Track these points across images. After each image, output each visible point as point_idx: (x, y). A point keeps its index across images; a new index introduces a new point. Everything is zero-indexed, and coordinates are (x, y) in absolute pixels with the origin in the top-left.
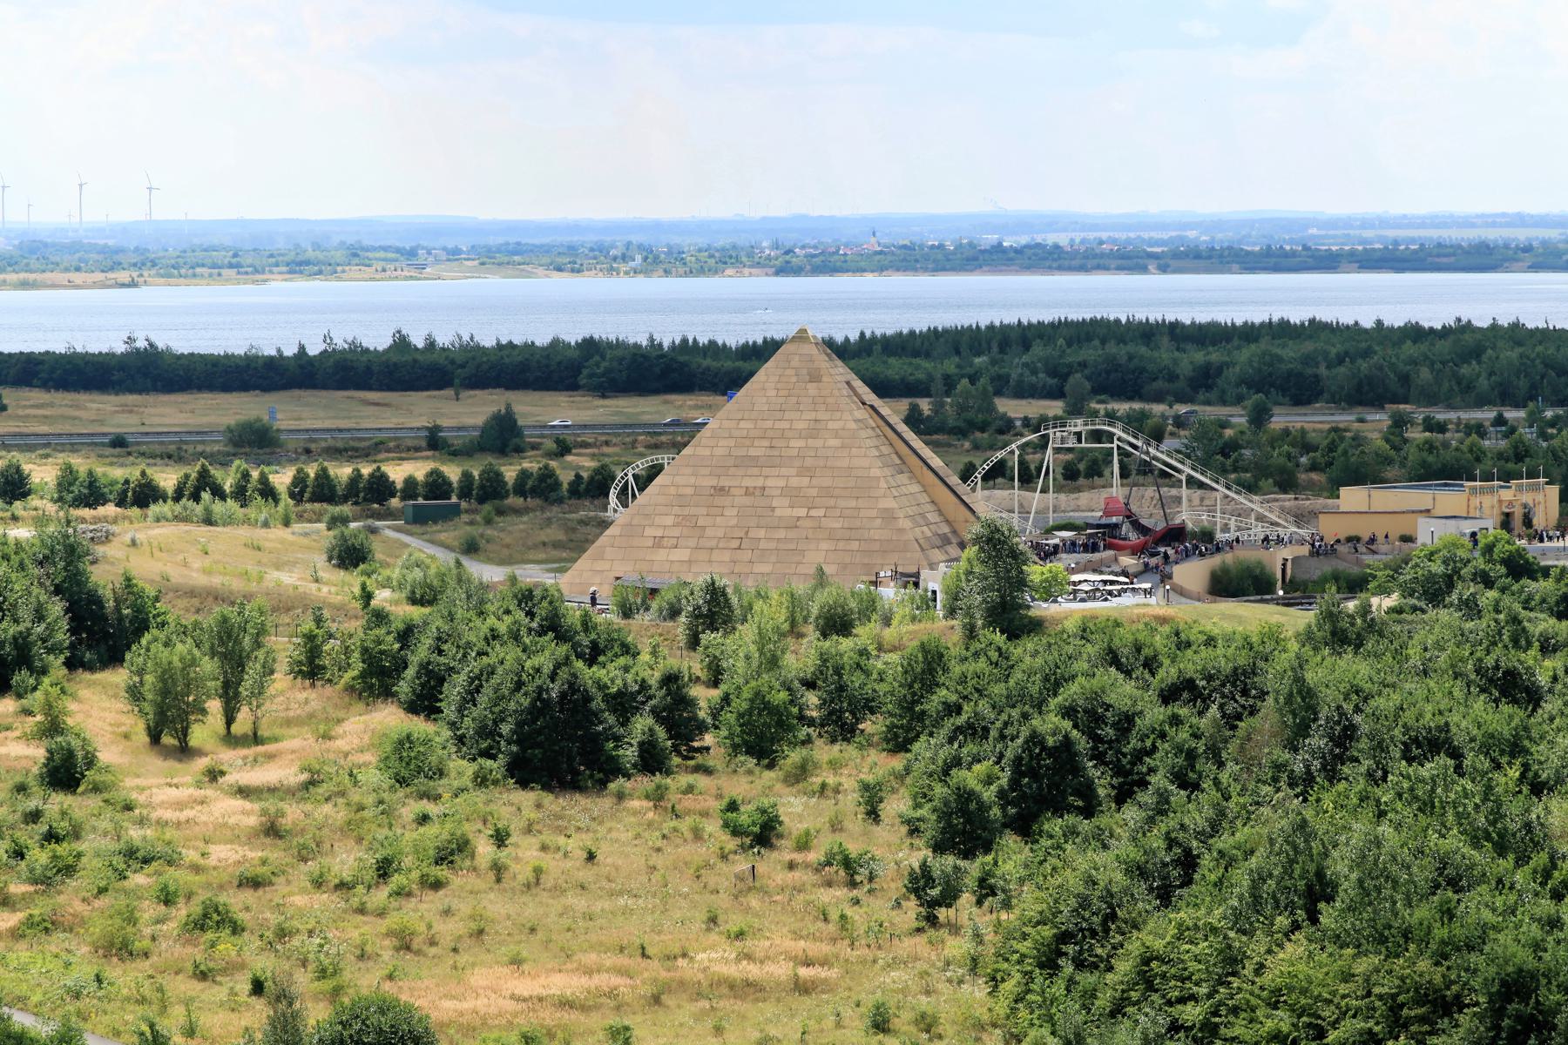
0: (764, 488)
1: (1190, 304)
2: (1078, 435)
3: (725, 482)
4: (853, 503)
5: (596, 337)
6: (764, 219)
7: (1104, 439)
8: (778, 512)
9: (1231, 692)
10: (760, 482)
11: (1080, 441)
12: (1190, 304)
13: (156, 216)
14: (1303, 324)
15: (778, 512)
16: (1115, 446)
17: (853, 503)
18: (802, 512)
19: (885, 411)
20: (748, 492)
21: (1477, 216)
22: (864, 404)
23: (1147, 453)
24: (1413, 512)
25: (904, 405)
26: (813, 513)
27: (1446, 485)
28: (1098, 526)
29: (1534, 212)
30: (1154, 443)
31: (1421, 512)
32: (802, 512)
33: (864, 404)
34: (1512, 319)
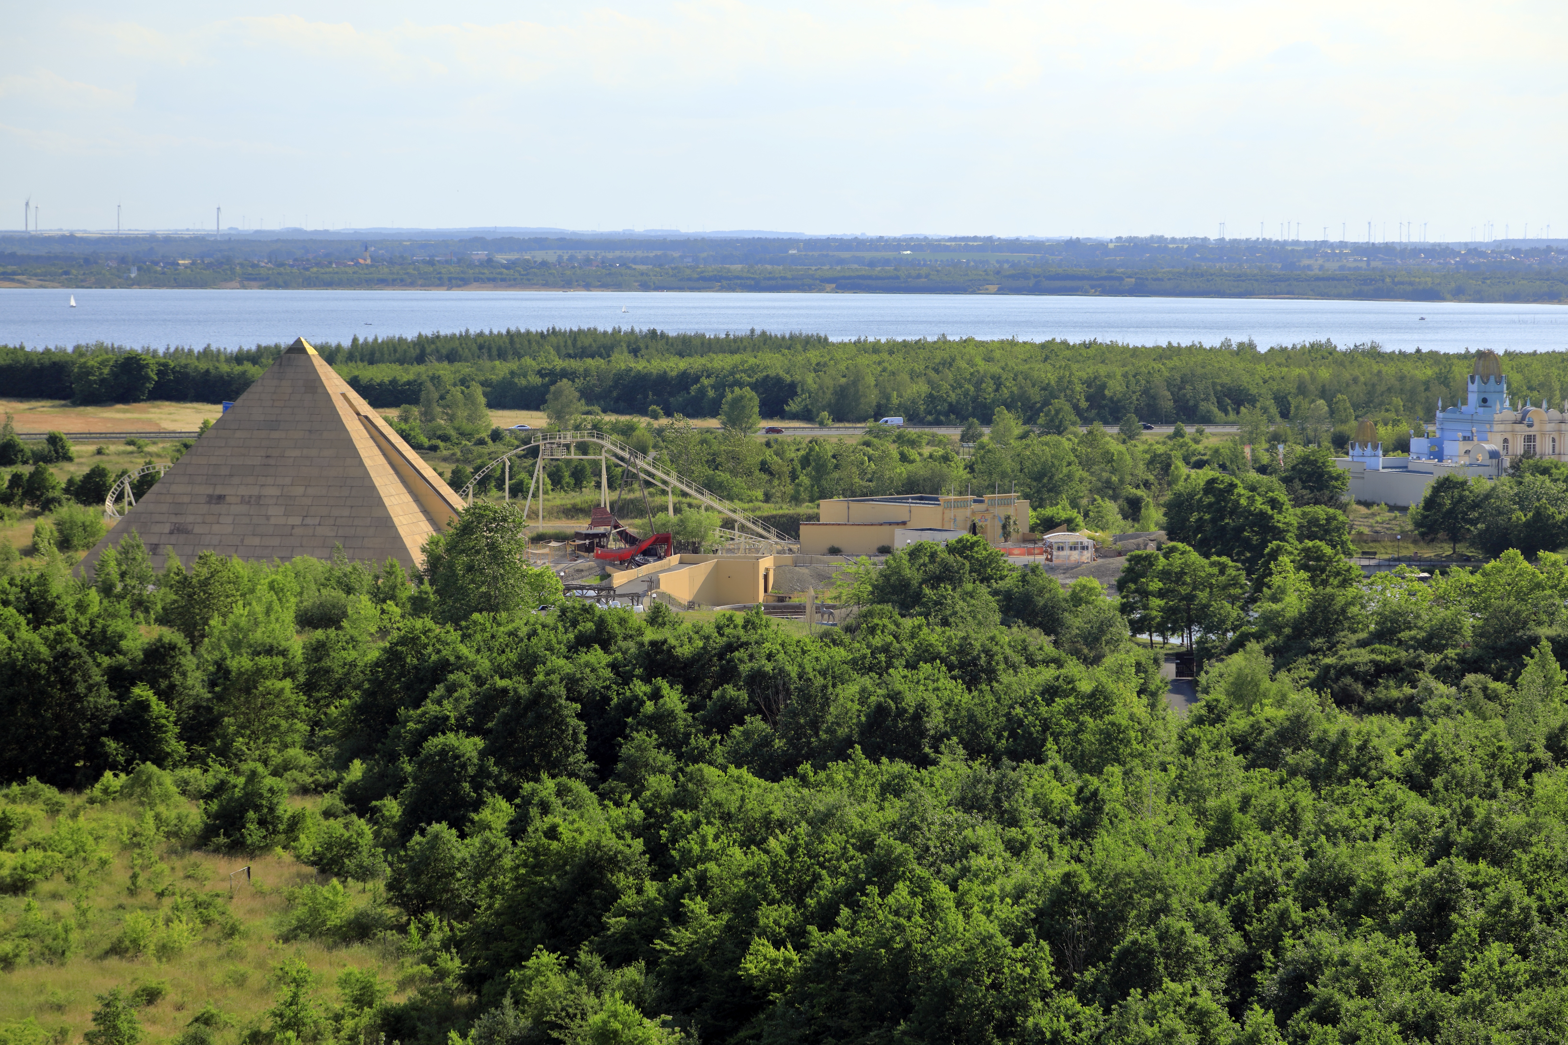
0: (259, 497)
1: (1028, 324)
2: (568, 446)
3: (219, 491)
4: (346, 512)
5: (52, 347)
6: (257, 232)
7: (591, 451)
8: (273, 521)
9: (1546, 698)
10: (255, 491)
11: (569, 452)
12: (1028, 324)
13: (31, 228)
14: (783, 338)
15: (273, 521)
16: (603, 457)
17: (346, 512)
18: (297, 521)
19: (380, 423)
20: (245, 500)
21: (951, 239)
22: (358, 414)
23: (635, 466)
24: (890, 524)
25: (394, 413)
26: (308, 521)
27: (921, 498)
28: (587, 536)
29: (1178, 235)
30: (640, 455)
31: (898, 524)
32: (297, 521)
33: (358, 414)
34: (416, 334)
